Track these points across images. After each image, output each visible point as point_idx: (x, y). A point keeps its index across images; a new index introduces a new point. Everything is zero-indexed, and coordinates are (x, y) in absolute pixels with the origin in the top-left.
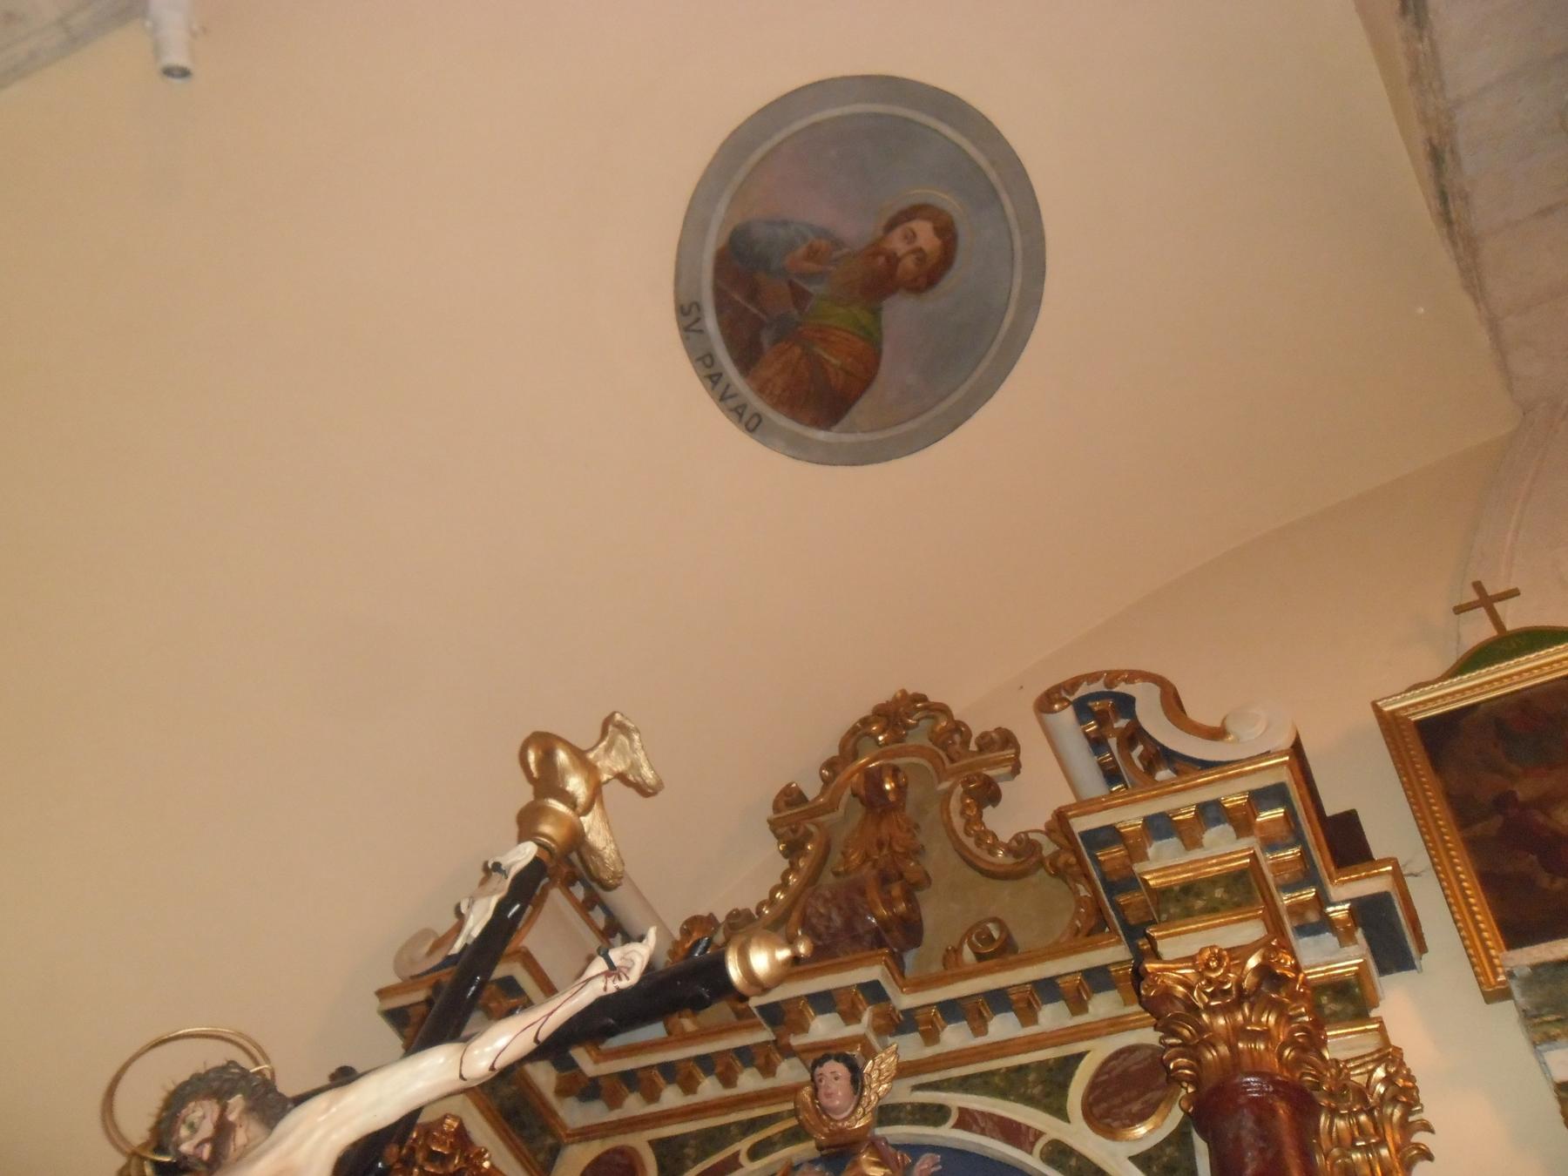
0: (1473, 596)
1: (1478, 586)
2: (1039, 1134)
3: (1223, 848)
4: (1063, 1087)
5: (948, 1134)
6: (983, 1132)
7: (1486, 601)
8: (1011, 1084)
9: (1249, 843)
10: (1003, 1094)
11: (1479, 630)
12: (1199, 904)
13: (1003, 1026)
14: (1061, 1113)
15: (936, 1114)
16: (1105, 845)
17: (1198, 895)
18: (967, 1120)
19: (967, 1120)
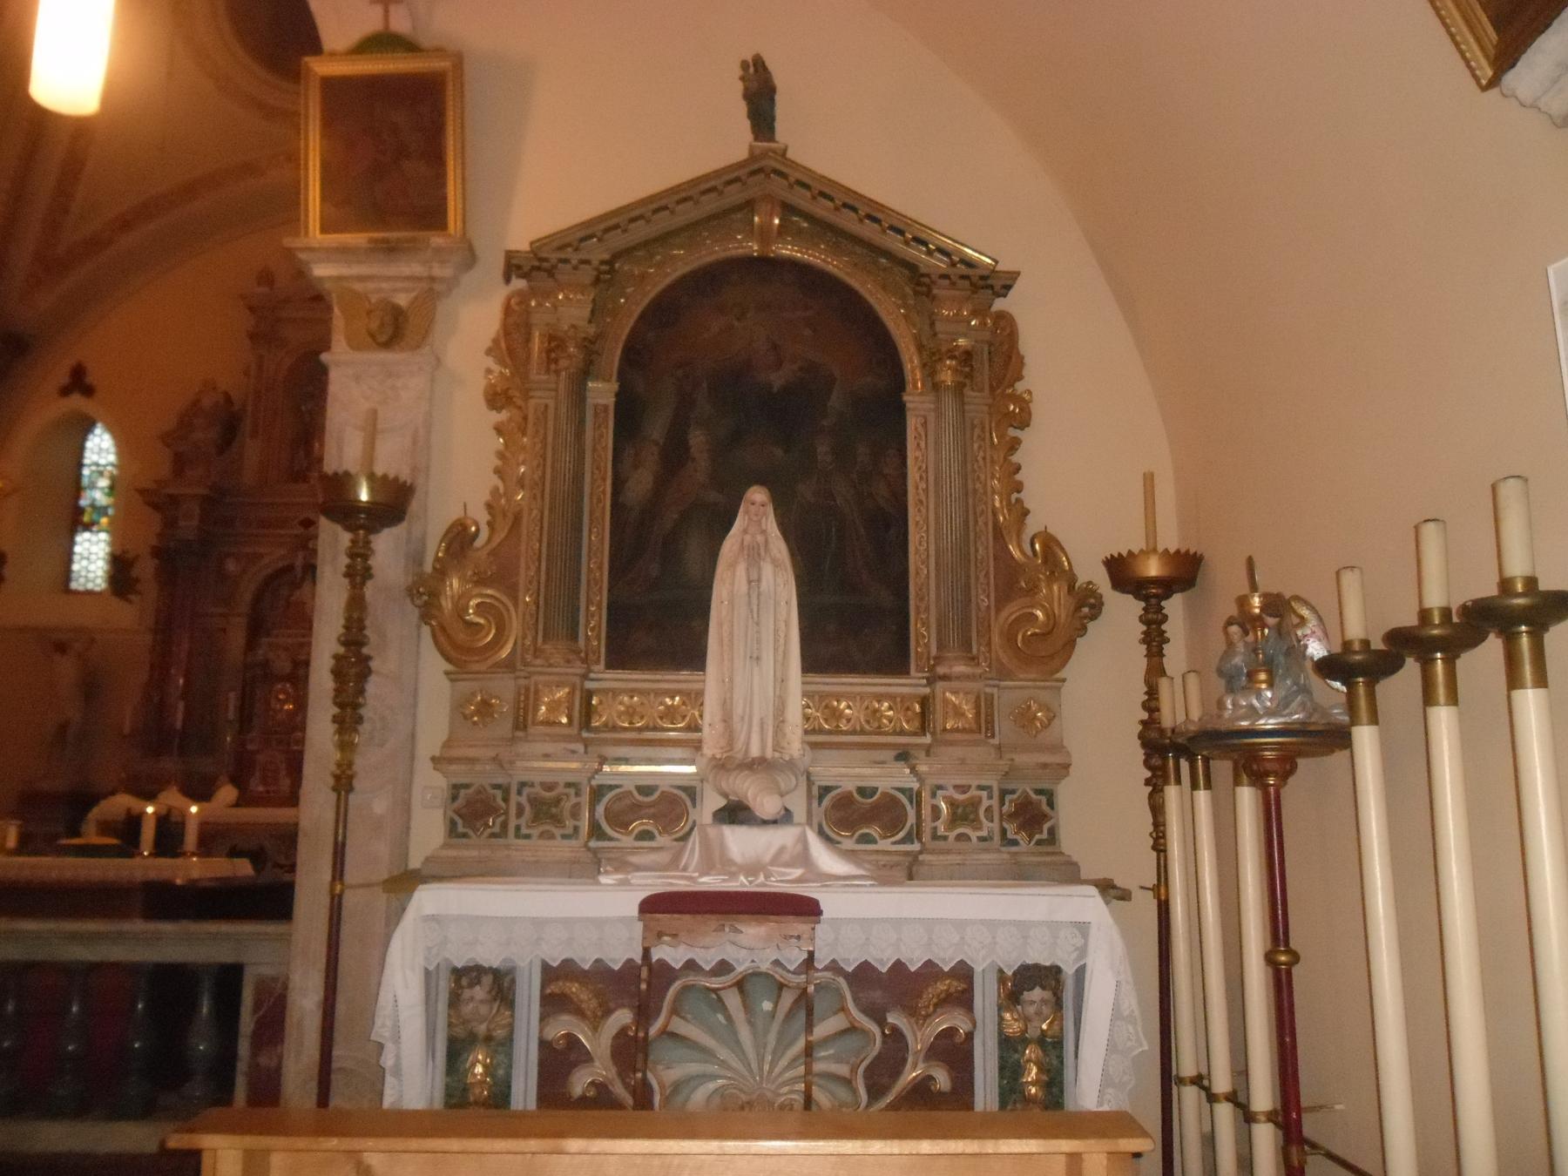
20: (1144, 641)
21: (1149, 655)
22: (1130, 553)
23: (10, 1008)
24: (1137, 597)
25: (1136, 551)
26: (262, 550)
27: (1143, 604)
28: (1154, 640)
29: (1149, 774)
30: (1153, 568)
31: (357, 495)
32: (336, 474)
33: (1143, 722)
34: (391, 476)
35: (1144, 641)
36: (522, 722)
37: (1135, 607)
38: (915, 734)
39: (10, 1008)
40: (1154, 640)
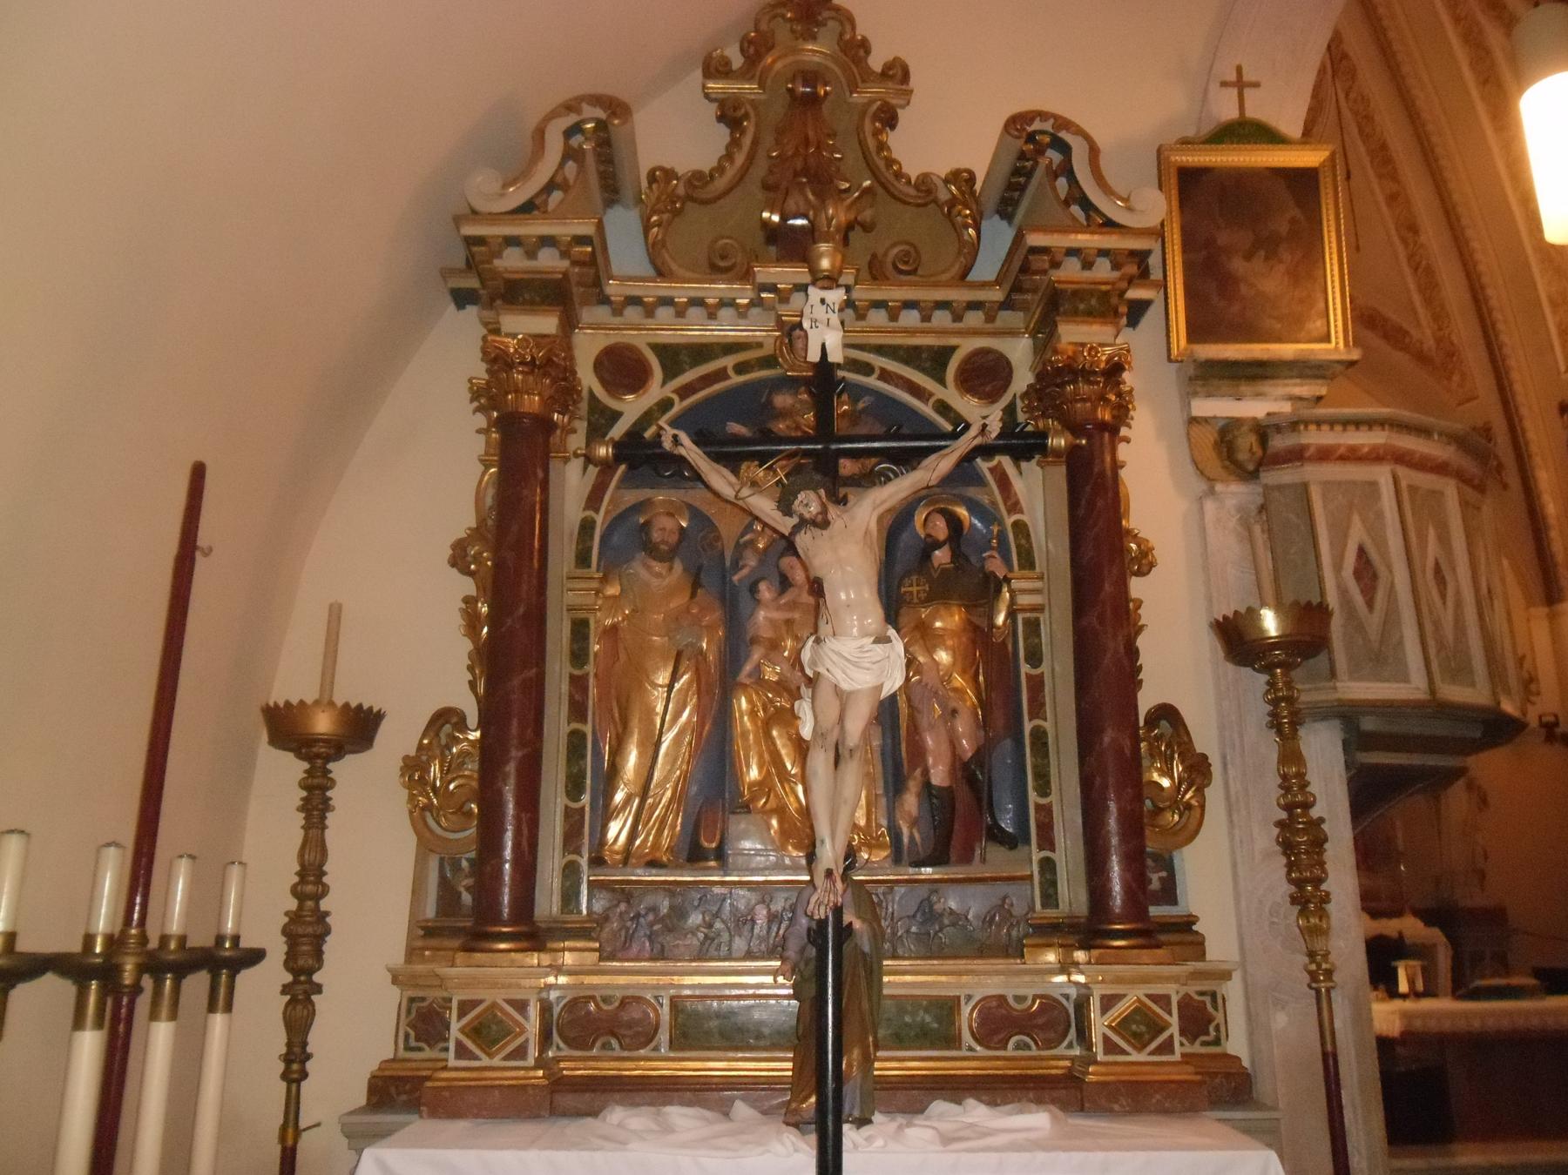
0: (1233, 77)
1: (1239, 70)
2: (931, 395)
3: (548, 260)
4: (944, 365)
5: (872, 381)
6: (897, 386)
7: (1240, 84)
8: (911, 356)
9: (565, 264)
10: (907, 362)
11: (1226, 109)
12: (1082, 306)
13: (910, 318)
14: (942, 381)
15: (867, 369)
16: (474, 244)
17: (1082, 300)
18: (885, 376)
19: (885, 376)
20: (301, 809)
21: (307, 828)
22: (302, 702)
23: (800, 222)
24: (300, 756)
25: (309, 701)
26: (674, 267)
27: (306, 765)
28: (316, 805)
29: (289, 978)
30: (323, 724)
31: (1261, 630)
32: (288, 704)
33: (1280, 824)
34: (353, 704)
35: (301, 809)
36: (1333, 674)
37: (292, 767)
38: (1032, 885)
39: (800, 222)
40: (316, 805)
